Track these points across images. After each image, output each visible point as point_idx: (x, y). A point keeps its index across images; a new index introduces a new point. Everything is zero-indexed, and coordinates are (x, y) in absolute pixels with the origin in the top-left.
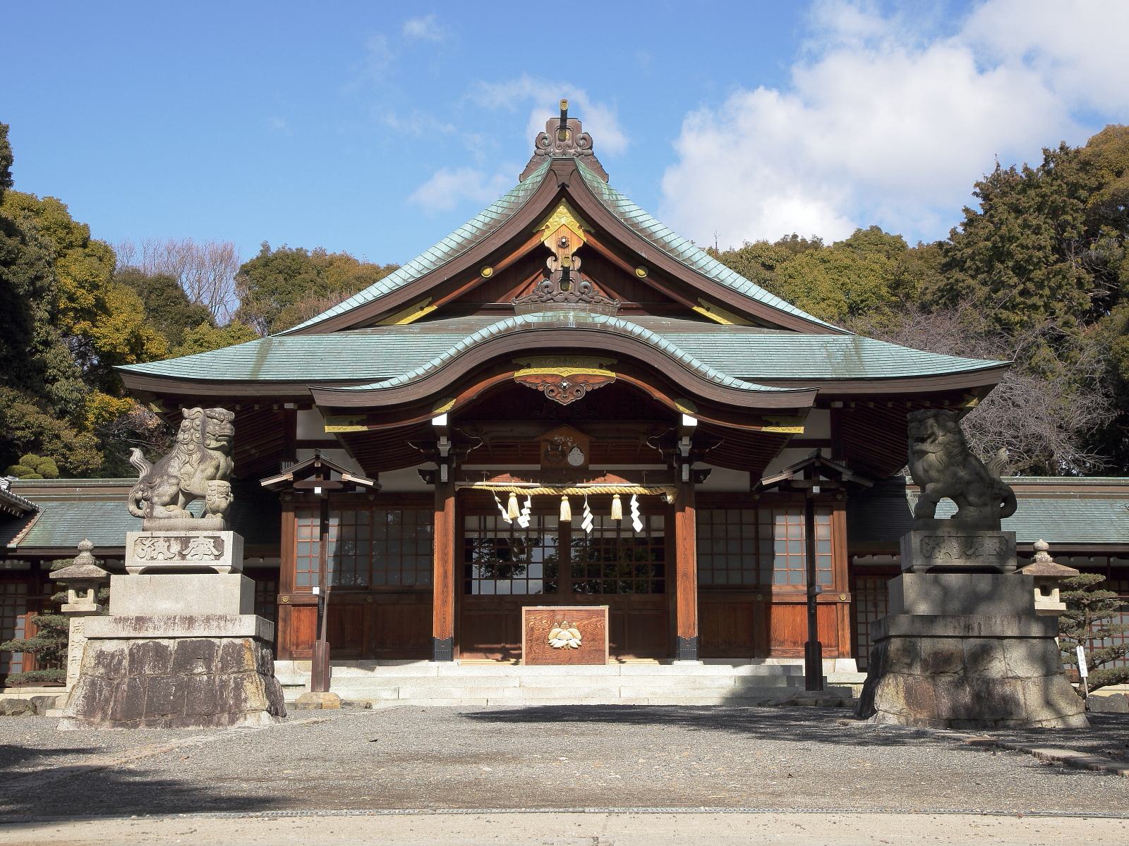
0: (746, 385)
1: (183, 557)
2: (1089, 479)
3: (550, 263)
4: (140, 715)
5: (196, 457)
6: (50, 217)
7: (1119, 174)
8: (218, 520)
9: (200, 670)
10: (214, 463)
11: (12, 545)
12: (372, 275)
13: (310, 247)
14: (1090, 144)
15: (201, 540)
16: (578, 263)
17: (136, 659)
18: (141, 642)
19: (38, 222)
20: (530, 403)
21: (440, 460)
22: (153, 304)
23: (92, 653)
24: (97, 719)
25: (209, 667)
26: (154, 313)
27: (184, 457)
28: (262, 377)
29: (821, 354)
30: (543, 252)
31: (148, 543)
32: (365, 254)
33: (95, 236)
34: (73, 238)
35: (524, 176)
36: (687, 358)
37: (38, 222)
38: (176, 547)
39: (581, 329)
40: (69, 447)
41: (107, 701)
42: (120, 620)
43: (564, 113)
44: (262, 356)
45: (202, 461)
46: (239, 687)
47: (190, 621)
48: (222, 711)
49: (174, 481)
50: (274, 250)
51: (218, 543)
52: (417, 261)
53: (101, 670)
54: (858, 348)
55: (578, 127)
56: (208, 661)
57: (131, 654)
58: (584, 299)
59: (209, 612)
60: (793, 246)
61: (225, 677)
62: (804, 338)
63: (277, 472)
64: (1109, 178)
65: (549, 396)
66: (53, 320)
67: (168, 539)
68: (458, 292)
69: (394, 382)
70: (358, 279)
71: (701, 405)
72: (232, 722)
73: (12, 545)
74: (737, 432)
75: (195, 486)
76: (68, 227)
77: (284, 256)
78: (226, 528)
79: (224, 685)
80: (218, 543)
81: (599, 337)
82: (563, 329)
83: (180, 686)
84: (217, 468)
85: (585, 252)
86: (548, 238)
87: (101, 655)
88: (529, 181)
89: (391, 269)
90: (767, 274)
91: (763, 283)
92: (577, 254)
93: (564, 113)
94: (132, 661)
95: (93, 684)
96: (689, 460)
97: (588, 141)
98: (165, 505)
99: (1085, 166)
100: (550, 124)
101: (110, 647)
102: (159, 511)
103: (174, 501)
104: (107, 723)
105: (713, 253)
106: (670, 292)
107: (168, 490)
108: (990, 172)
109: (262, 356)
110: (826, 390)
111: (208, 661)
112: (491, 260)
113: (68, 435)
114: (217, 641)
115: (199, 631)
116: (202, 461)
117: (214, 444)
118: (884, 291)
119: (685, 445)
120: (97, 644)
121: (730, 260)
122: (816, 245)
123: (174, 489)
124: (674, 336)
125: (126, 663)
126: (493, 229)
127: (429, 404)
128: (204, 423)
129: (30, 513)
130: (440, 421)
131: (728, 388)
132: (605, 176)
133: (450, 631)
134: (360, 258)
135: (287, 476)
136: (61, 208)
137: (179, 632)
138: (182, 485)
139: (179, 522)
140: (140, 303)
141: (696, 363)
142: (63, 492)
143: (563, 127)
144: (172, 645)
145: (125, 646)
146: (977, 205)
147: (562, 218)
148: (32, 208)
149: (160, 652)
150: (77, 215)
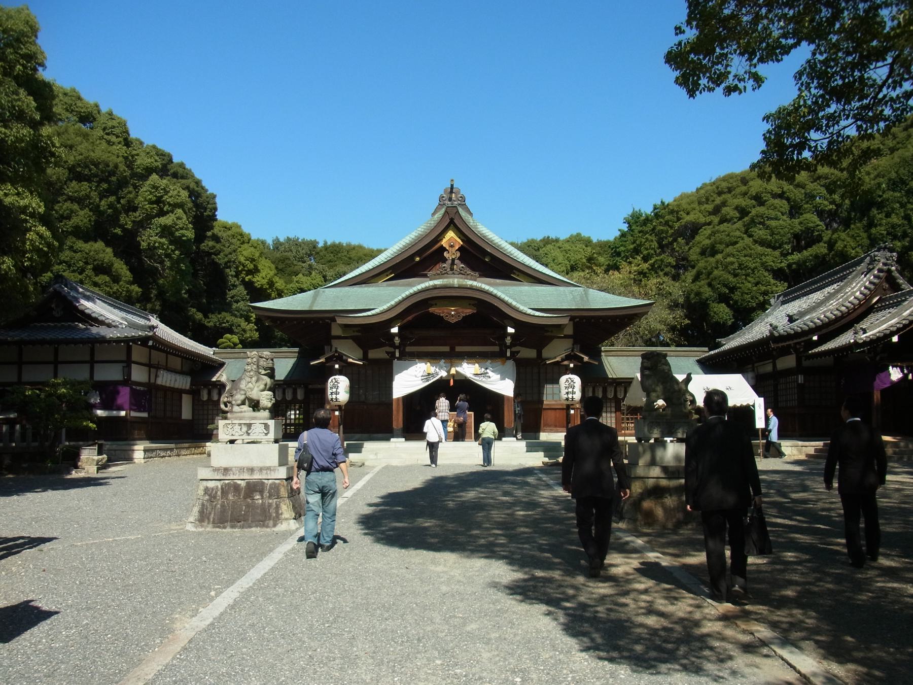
0: (537, 314)
1: (249, 434)
2: (679, 349)
3: (445, 254)
4: (227, 521)
5: (254, 379)
6: (234, 230)
7: (688, 214)
8: (266, 414)
9: (258, 497)
10: (264, 382)
11: (214, 379)
12: (372, 254)
13: (344, 242)
14: (675, 201)
15: (258, 425)
16: (458, 254)
17: (225, 491)
18: (227, 482)
19: (230, 233)
20: (438, 322)
21: (395, 347)
22: (280, 267)
23: (202, 488)
24: (205, 524)
25: (262, 496)
26: (280, 271)
27: (248, 379)
28: (314, 309)
29: (570, 297)
30: (443, 249)
31: (230, 427)
32: (370, 244)
33: (254, 237)
34: (244, 239)
35: (433, 214)
36: (506, 299)
37: (230, 233)
38: (245, 429)
39: (461, 287)
40: (244, 331)
41: (210, 514)
42: (216, 470)
43: (452, 186)
44: (315, 298)
45: (257, 381)
46: (278, 507)
47: (251, 470)
48: (270, 519)
49: (243, 392)
50: (329, 243)
51: (266, 426)
52: (393, 244)
53: (207, 497)
54: (586, 294)
55: (459, 192)
56: (261, 492)
57: (222, 488)
58: (461, 273)
59: (261, 465)
60: (547, 241)
61: (270, 501)
62: (561, 289)
63: (318, 359)
64: (684, 215)
65: (446, 319)
66: (237, 276)
67: (240, 424)
68: (404, 268)
69: (377, 311)
70: (365, 255)
71: (516, 323)
72: (275, 525)
73: (214, 379)
74: (534, 334)
75: (255, 394)
76: (242, 235)
77: (334, 245)
78: (272, 418)
79: (270, 505)
80: (266, 426)
81: (469, 291)
82: (451, 287)
83: (248, 506)
84: (266, 385)
85: (461, 249)
86: (444, 242)
87: (206, 490)
88: (436, 216)
89: (380, 252)
90: (535, 253)
91: (538, 260)
92: (459, 250)
93: (452, 186)
94: (222, 492)
95: (203, 505)
96: (510, 347)
97: (463, 198)
98: (238, 405)
99: (672, 212)
100: (445, 191)
101: (211, 484)
102: (236, 409)
103: (243, 403)
104: (211, 525)
105: (512, 244)
106: (501, 268)
107: (239, 397)
108: (630, 213)
109: (315, 298)
110: (574, 314)
111: (261, 492)
112: (418, 253)
113: (244, 324)
114: (266, 481)
115: (257, 476)
116: (257, 381)
117: (263, 372)
118: (584, 260)
119: (508, 340)
120: (205, 483)
121: (522, 248)
122: (557, 240)
123: (243, 397)
124: (502, 288)
125: (219, 493)
126: (420, 239)
127: (390, 323)
128: (258, 361)
129: (222, 365)
130: (395, 330)
131: (529, 315)
132: (471, 214)
133: (401, 425)
134: (366, 245)
135: (322, 360)
136: (240, 227)
137: (246, 476)
138: (248, 394)
139: (246, 414)
140: (273, 266)
141: (514, 303)
142: (236, 355)
143: (451, 192)
144: (243, 483)
145: (219, 484)
146: (625, 227)
147: (451, 234)
148: (227, 228)
149: (237, 488)
150: (246, 229)
